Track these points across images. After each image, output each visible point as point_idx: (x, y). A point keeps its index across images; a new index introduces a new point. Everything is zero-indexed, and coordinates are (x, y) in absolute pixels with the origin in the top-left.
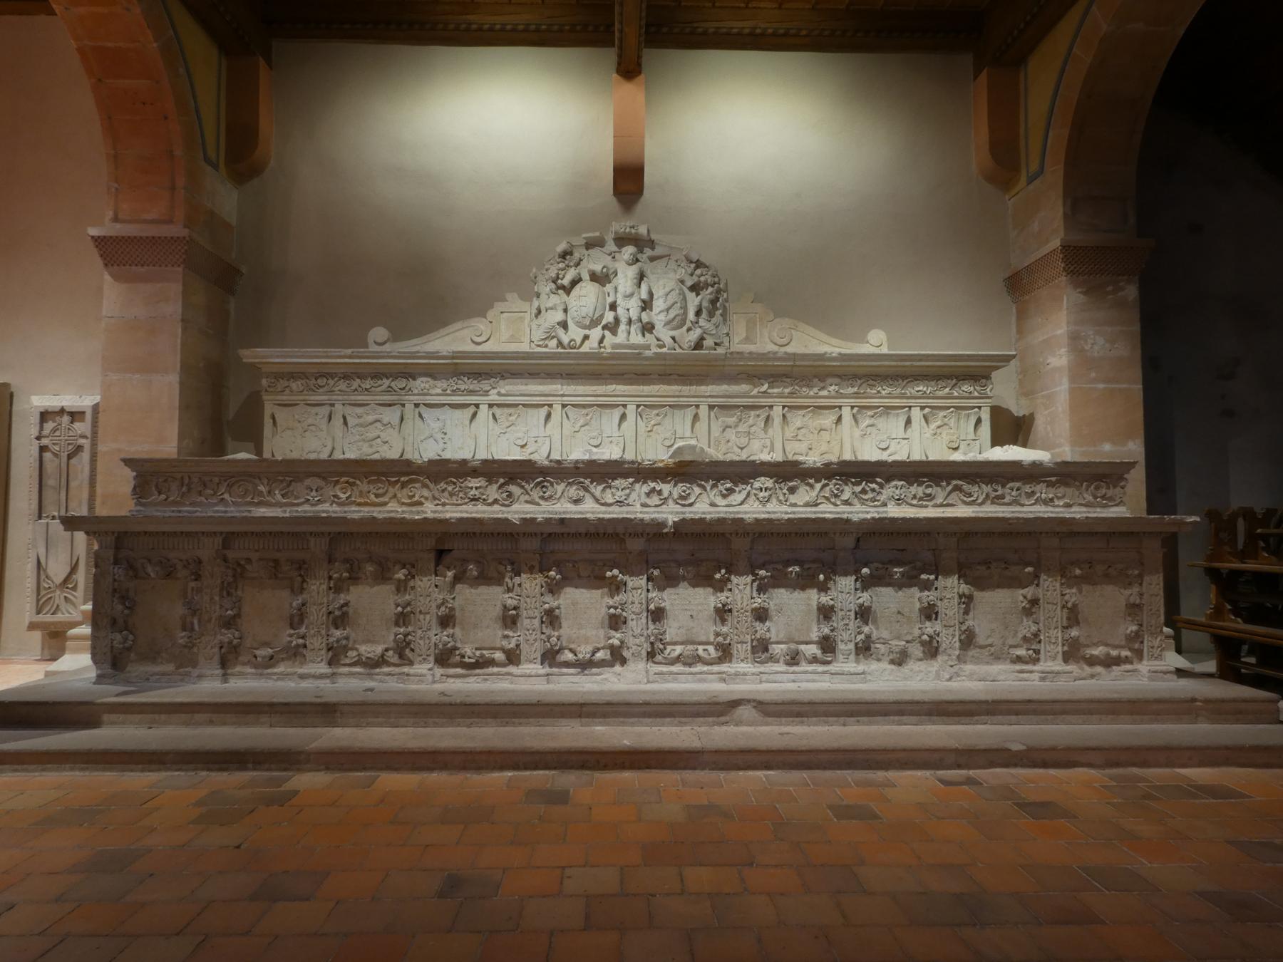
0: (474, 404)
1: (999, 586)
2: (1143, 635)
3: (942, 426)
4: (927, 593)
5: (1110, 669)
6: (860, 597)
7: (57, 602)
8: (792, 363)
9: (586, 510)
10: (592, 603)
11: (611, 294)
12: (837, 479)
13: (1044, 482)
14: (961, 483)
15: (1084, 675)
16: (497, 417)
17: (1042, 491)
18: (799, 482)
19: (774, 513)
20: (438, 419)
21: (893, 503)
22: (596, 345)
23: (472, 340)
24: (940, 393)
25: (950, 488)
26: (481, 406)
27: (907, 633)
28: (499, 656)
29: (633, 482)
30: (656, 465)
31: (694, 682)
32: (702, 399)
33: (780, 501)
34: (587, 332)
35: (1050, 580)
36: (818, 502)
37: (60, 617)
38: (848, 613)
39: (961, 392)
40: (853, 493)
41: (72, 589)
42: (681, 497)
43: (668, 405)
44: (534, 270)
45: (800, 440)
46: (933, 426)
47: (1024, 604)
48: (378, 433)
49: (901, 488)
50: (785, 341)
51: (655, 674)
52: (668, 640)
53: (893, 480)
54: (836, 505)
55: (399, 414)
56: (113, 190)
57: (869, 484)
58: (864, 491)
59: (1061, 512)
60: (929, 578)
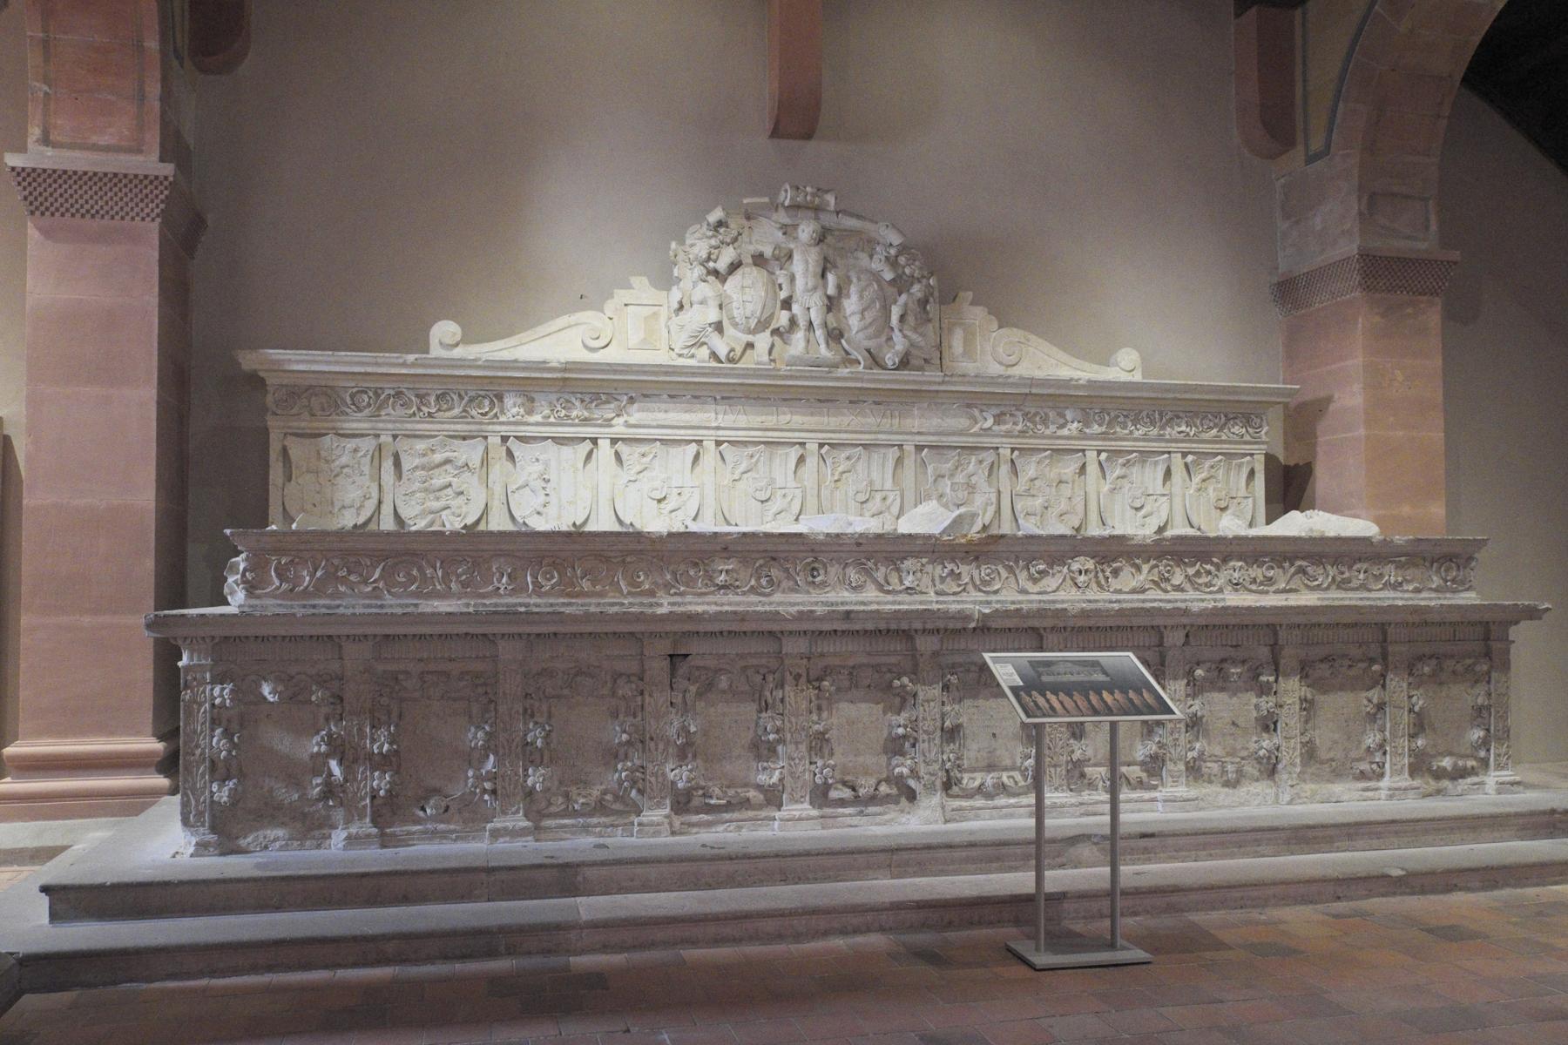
0: (590, 438)
1: (1342, 688)
3: (1208, 479)
4: (1264, 698)
5: (1456, 783)
8: (1027, 391)
9: (869, 599)
10: (872, 722)
11: (784, 286)
12: (1167, 559)
13: (1395, 562)
14: (1304, 563)
17: (1391, 573)
19: (1096, 601)
20: (537, 460)
21: (1230, 588)
22: (766, 358)
25: (1293, 570)
26: (599, 441)
27: (1243, 748)
28: (752, 794)
30: (957, 541)
31: (1001, 818)
32: (906, 437)
34: (750, 338)
43: (861, 445)
45: (1033, 496)
46: (1197, 479)
47: (1368, 709)
48: (449, 479)
50: (1013, 359)
51: (953, 810)
52: (966, 766)
53: (1231, 560)
54: (1166, 591)
55: (481, 449)
58: (1198, 574)
59: (1411, 599)
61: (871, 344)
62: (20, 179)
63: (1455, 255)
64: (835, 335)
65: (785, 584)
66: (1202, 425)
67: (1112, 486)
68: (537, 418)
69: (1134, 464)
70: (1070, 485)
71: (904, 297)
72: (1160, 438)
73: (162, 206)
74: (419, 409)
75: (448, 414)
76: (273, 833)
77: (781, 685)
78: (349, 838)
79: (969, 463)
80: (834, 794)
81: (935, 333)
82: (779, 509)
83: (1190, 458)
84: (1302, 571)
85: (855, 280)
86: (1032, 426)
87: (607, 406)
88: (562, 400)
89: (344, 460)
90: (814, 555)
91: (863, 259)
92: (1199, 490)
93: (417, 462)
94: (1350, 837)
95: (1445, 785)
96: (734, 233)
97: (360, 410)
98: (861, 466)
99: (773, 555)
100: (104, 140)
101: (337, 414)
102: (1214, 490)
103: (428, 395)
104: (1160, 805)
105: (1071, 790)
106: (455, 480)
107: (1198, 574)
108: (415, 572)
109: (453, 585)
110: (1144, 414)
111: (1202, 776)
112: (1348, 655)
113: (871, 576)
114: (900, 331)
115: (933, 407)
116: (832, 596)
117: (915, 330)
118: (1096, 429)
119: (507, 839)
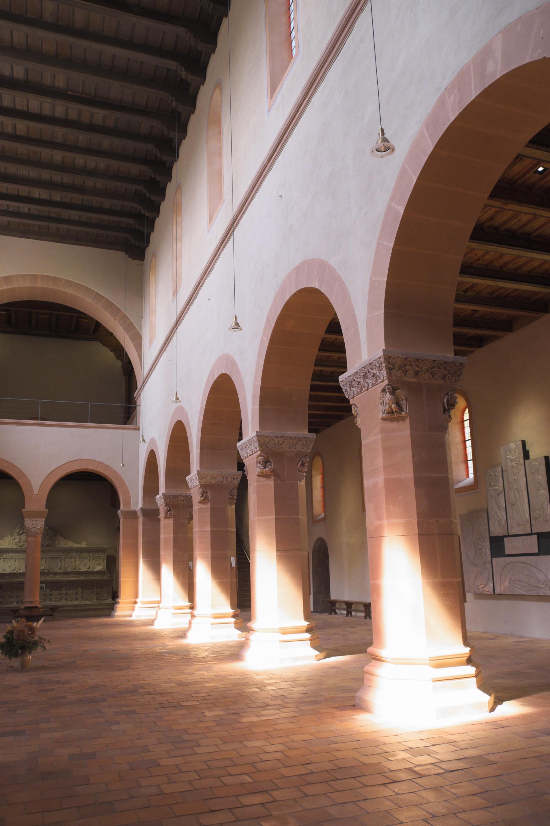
28: (9, 602)
72: (88, 555)
80: (19, 602)
116: (19, 580)
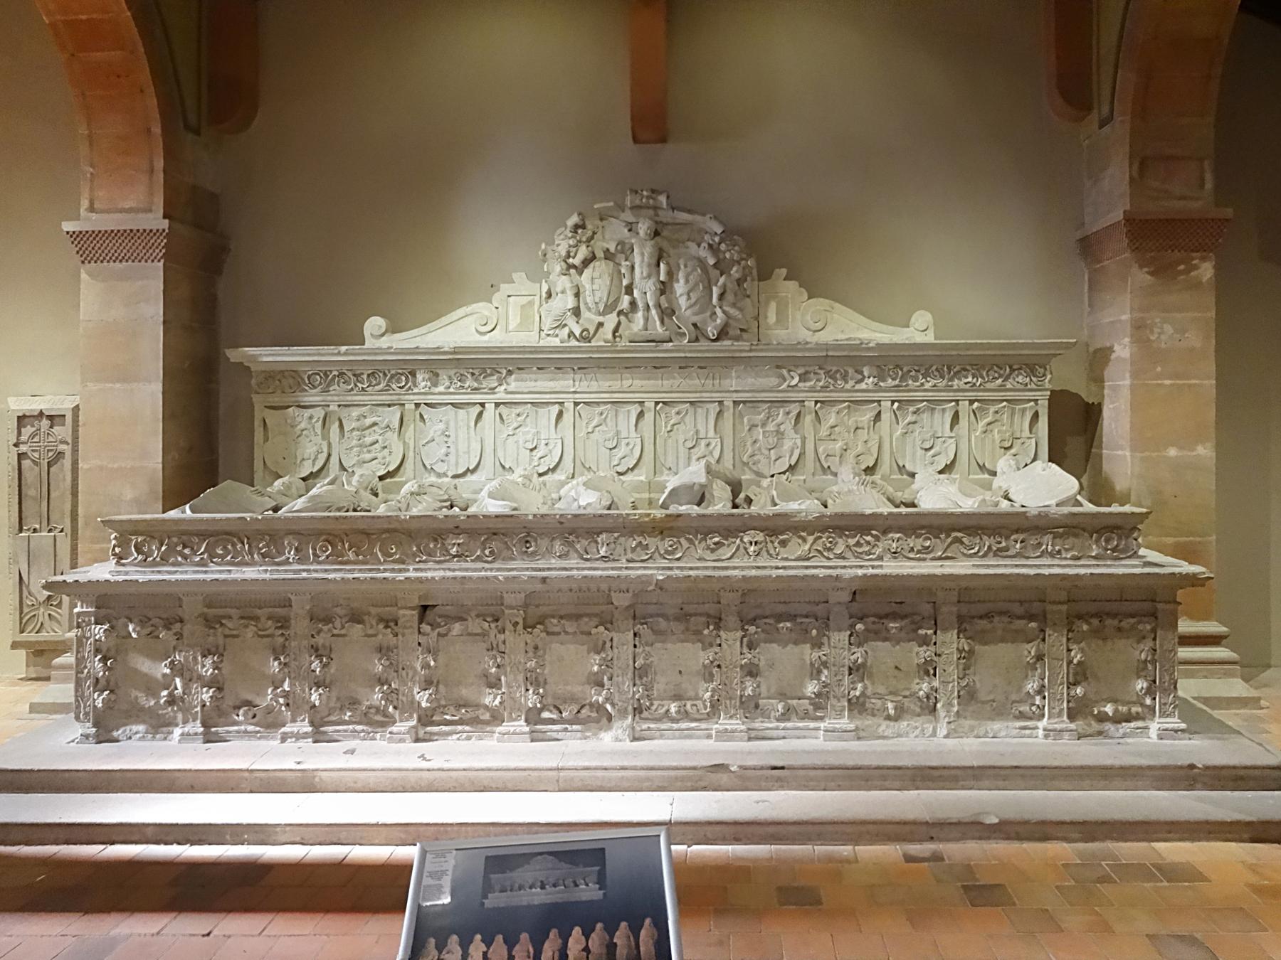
1: (1003, 640)
2: (1156, 692)
4: (925, 648)
5: (1119, 726)
6: (854, 653)
7: (41, 619)
8: (824, 354)
12: (830, 532)
13: (1051, 533)
14: (959, 535)
15: (1090, 731)
16: (505, 418)
18: (791, 535)
21: (889, 556)
23: (477, 331)
24: (988, 386)
25: (949, 540)
26: (486, 405)
29: (619, 537)
30: (641, 520)
32: (724, 395)
33: (771, 555)
34: (601, 319)
35: (1056, 634)
36: (811, 555)
37: (44, 635)
38: (841, 669)
39: (1016, 384)
40: (847, 546)
41: (56, 606)
42: (667, 552)
44: (543, 246)
45: (834, 440)
46: (982, 423)
48: (377, 437)
49: (898, 541)
50: (819, 326)
53: (890, 532)
54: (828, 559)
56: (89, 175)
57: (865, 537)
58: (858, 544)
60: (926, 633)
61: (695, 319)
62: (72, 239)
63: (1229, 212)
64: (667, 313)
65: (506, 553)
66: (988, 376)
67: (905, 431)
68: (441, 389)
69: (924, 412)
70: (866, 430)
71: (722, 280)
72: (948, 389)
73: (164, 251)
74: (356, 385)
75: (377, 388)
76: (135, 728)
77: (503, 631)
78: (182, 734)
79: (778, 414)
80: (546, 715)
81: (753, 306)
82: (623, 455)
83: (976, 404)
84: (959, 541)
85: (682, 267)
86: (832, 382)
87: (492, 378)
88: (458, 375)
89: (303, 425)
90: (526, 530)
91: (692, 246)
92: (985, 432)
93: (354, 425)
94: (976, 778)
95: (1107, 728)
96: (590, 233)
97: (315, 387)
98: (689, 419)
99: (495, 531)
100: (127, 205)
101: (300, 391)
102: (999, 432)
103: (363, 374)
104: (822, 732)
105: (746, 718)
106: (381, 437)
107: (858, 544)
108: (229, 547)
109: (255, 556)
110: (934, 368)
111: (866, 710)
112: (1008, 612)
113: (574, 547)
114: (720, 307)
115: (749, 368)
117: (734, 305)
118: (890, 382)
119: (294, 740)
